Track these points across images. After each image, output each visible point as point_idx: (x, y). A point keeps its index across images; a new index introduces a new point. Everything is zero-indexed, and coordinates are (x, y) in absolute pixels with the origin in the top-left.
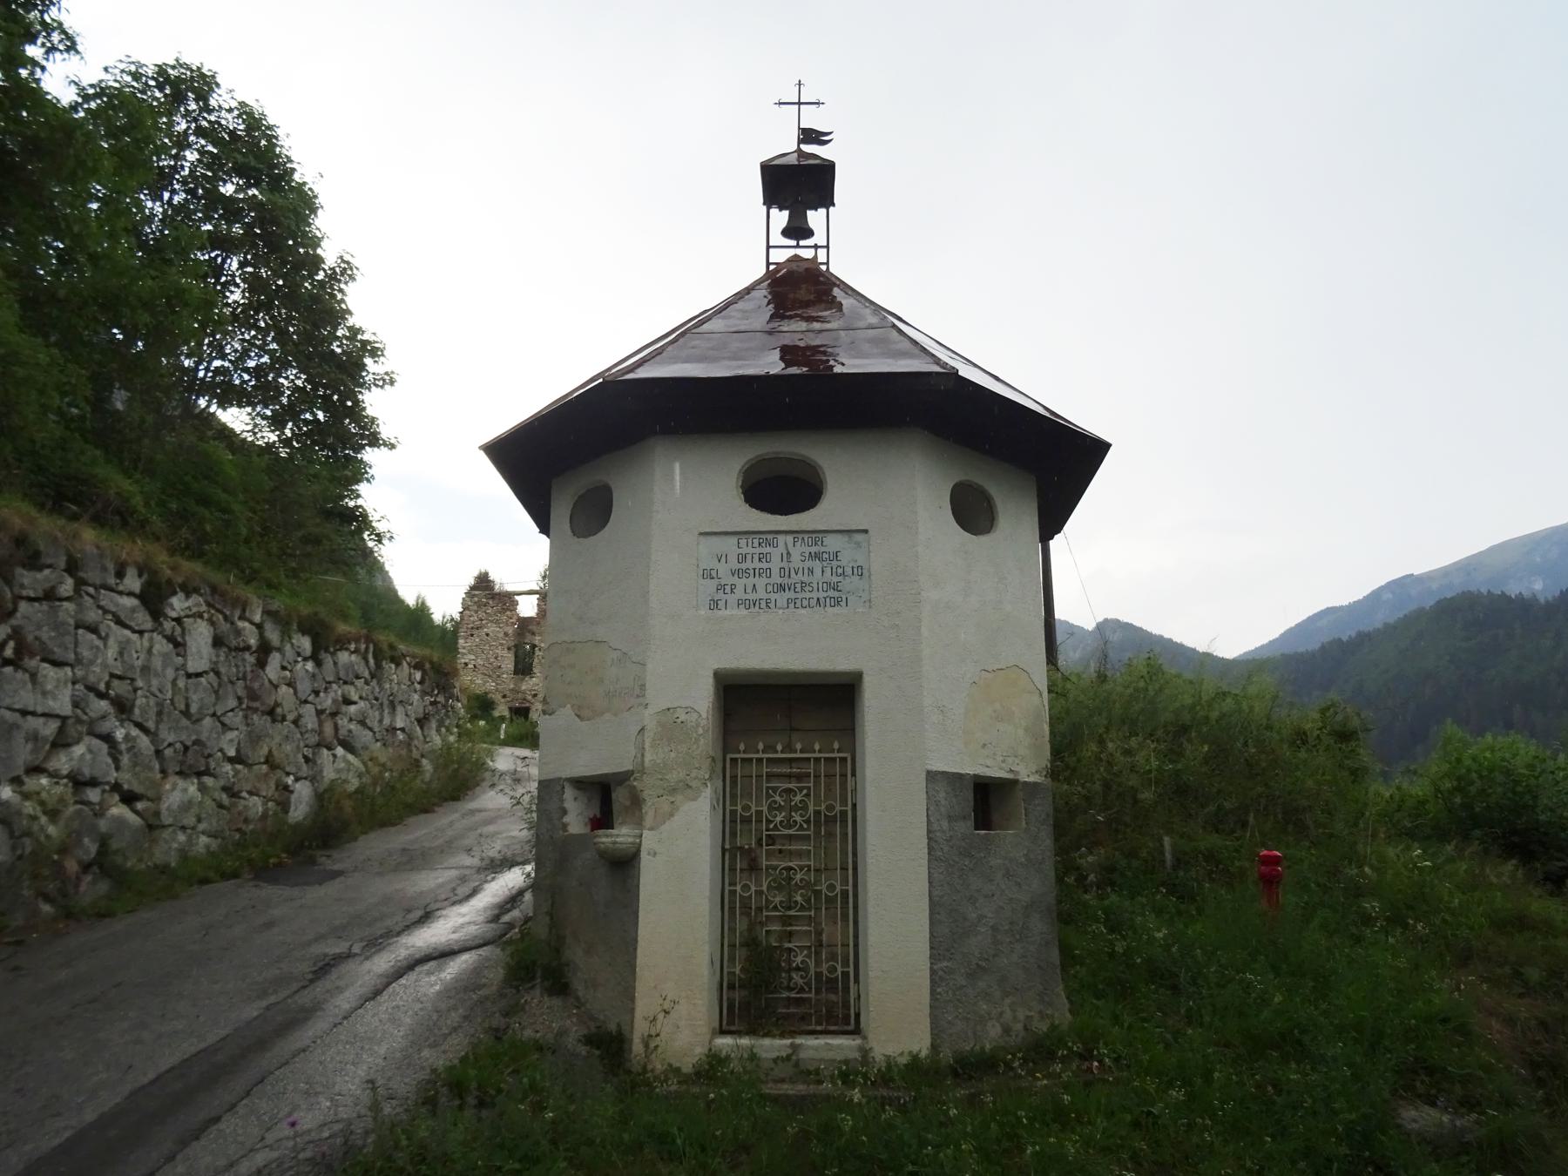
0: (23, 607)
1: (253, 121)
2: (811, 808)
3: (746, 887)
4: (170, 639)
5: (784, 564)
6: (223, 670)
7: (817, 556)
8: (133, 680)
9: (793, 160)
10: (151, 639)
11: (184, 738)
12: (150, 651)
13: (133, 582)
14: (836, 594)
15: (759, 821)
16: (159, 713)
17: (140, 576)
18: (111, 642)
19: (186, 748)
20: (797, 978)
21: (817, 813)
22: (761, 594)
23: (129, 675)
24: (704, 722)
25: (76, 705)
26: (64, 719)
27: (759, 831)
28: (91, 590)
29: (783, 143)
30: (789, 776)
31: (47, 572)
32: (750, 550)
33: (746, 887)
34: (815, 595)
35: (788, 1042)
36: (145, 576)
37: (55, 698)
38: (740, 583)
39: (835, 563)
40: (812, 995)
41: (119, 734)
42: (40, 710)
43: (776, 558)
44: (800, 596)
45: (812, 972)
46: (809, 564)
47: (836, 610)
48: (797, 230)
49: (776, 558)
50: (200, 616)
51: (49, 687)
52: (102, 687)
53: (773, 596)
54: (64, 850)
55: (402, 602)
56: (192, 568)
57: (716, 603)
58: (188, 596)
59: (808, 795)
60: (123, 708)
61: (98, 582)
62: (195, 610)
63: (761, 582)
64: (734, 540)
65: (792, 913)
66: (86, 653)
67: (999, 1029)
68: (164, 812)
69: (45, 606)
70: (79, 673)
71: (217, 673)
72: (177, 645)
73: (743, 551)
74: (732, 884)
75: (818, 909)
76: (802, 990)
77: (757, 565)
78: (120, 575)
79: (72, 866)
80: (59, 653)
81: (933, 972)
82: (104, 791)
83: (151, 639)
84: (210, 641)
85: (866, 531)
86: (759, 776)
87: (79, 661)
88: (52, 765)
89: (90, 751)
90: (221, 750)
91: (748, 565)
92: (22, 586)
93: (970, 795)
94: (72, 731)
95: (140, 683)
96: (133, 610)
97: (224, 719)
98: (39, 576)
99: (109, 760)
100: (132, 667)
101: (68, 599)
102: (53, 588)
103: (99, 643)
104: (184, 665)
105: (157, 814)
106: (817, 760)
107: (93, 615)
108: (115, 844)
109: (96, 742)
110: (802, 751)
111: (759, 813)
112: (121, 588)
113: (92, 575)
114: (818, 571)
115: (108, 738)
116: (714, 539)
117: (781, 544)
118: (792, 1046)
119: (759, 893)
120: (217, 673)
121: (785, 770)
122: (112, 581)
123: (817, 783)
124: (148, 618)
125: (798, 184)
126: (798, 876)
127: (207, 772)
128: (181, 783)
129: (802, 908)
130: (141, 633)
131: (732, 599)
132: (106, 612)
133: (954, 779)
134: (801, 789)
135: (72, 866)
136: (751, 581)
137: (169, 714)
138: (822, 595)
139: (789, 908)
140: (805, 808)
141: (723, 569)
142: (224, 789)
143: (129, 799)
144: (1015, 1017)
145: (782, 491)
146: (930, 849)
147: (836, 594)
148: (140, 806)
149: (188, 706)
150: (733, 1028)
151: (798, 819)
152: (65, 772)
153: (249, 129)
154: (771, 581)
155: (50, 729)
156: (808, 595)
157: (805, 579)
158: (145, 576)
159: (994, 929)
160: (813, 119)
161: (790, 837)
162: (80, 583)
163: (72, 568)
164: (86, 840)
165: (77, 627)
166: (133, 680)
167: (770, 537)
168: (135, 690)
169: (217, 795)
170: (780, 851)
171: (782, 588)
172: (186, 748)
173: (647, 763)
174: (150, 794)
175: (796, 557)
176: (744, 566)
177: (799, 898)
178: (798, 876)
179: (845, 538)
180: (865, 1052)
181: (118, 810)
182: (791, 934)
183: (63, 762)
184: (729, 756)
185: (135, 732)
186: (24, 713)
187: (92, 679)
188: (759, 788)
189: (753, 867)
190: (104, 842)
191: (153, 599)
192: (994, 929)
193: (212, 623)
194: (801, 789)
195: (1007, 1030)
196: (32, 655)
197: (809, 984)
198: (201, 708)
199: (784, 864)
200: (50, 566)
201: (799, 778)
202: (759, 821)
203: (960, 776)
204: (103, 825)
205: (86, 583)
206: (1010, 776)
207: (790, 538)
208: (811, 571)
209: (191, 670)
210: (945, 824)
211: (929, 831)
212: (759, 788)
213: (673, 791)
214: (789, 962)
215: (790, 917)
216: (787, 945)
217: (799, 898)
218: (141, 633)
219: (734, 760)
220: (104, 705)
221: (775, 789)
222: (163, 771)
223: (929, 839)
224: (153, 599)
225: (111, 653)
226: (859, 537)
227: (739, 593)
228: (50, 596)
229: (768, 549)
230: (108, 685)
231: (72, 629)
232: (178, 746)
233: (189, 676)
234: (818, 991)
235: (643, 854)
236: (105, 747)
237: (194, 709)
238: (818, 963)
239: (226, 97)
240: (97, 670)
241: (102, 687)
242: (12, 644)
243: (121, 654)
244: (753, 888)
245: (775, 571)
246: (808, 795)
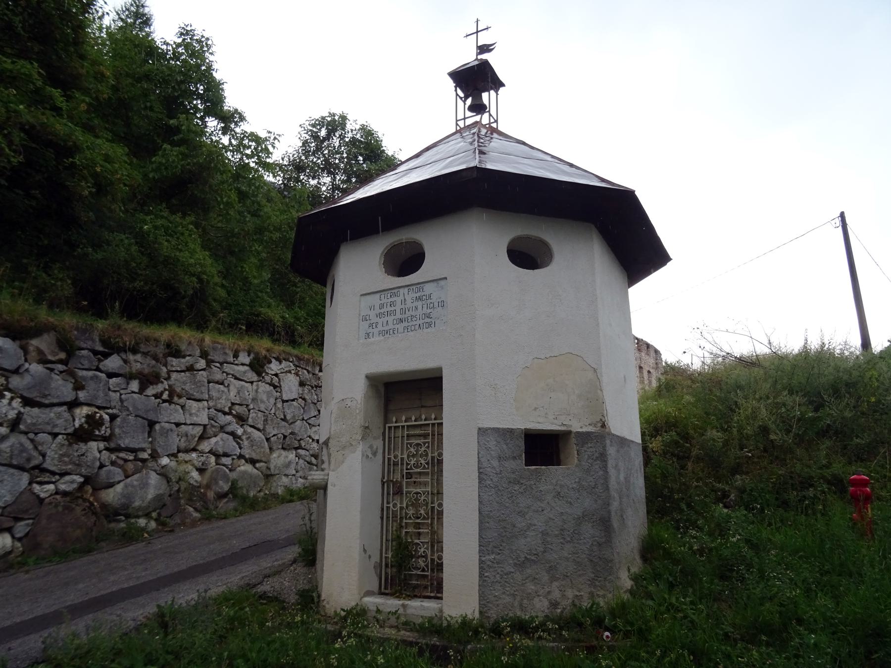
0: (174, 376)
1: (367, 132)
2: (430, 455)
3: (395, 505)
4: (271, 384)
5: (403, 306)
6: (307, 397)
7: (419, 299)
8: (247, 406)
9: (477, 63)
10: (257, 385)
11: (283, 431)
12: (257, 391)
13: (244, 358)
14: (429, 320)
15: (402, 464)
16: (266, 420)
17: (249, 355)
18: (231, 387)
19: (285, 437)
20: (421, 563)
21: (433, 458)
22: (391, 326)
23: (244, 403)
24: (359, 406)
25: (210, 418)
26: (205, 426)
27: (402, 470)
28: (218, 365)
29: (467, 56)
30: (420, 435)
31: (188, 358)
32: (386, 301)
33: (395, 505)
34: (418, 322)
35: (401, 602)
36: (252, 356)
37: (197, 416)
38: (380, 321)
39: (429, 301)
40: (429, 574)
41: (240, 431)
42: (188, 422)
43: (399, 303)
44: (410, 324)
45: (429, 559)
46: (416, 304)
47: (429, 330)
48: (478, 108)
49: (399, 303)
50: (290, 372)
51: (194, 411)
52: (227, 410)
53: (396, 326)
54: (208, 487)
55: (842, 358)
56: (279, 348)
57: (368, 334)
58: (280, 362)
59: (428, 447)
60: (241, 420)
61: (221, 361)
62: (287, 369)
63: (390, 319)
64: (378, 295)
65: (418, 521)
66: (214, 394)
67: (546, 603)
68: (272, 467)
69: (188, 374)
70: (211, 404)
71: (304, 399)
72: (275, 387)
73: (382, 302)
74: (388, 503)
75: (433, 519)
76: (423, 570)
77: (389, 309)
78: (236, 356)
79: (211, 495)
80: (197, 395)
81: (481, 562)
82: (233, 459)
83: (257, 385)
84: (297, 383)
85: (446, 278)
86: (403, 437)
87: (211, 398)
88: (200, 448)
89: (222, 439)
90: (310, 437)
91: (385, 310)
92: (172, 366)
93: (522, 444)
94: (210, 431)
95: (251, 406)
96: (245, 372)
97: (309, 421)
98: (183, 360)
99: (235, 444)
100: (245, 399)
101: (204, 370)
102: (192, 366)
103: (226, 390)
104: (281, 396)
105: (268, 468)
106: (433, 424)
107: (218, 376)
108: (240, 484)
109: (225, 435)
110: (415, 421)
111: (402, 459)
112: (236, 362)
113: (216, 356)
114: (420, 307)
115: (233, 434)
116: (368, 297)
117: (402, 295)
118: (404, 606)
119: (402, 508)
120: (304, 399)
121: (418, 432)
122: (231, 359)
123: (433, 439)
124: (255, 375)
125: (476, 80)
126: (422, 498)
127: (300, 447)
128: (284, 453)
129: (424, 518)
130: (252, 383)
131: (376, 331)
132: (228, 374)
133: (507, 434)
134: (425, 443)
135: (211, 495)
136: (386, 318)
137: (272, 420)
138: (421, 322)
139: (418, 518)
140: (427, 455)
141: (372, 314)
142: (312, 455)
143: (253, 462)
144: (563, 596)
145: (406, 262)
146: (481, 480)
147: (429, 320)
148: (257, 465)
149: (285, 416)
150: (387, 591)
151: (423, 462)
152: (207, 451)
153: (367, 137)
154: (396, 317)
155: (198, 430)
156: (414, 323)
157: (413, 313)
158: (252, 356)
159: (544, 534)
160: (484, 39)
161: (420, 473)
162: (209, 363)
163: (204, 355)
164: (221, 482)
165: (209, 382)
166: (247, 406)
167: (396, 291)
168: (249, 411)
169: (307, 459)
170: (415, 482)
171: (401, 321)
172: (285, 437)
173: (332, 433)
174: (263, 459)
175: (409, 301)
176: (382, 311)
177: (422, 512)
178: (422, 498)
179: (435, 284)
180: (441, 611)
181: (248, 468)
182: (419, 534)
183: (205, 446)
184: (387, 425)
185: (250, 430)
186: (178, 425)
187: (219, 406)
188: (402, 443)
189: (399, 492)
190: (234, 484)
191: (258, 366)
192: (544, 534)
193: (297, 374)
194: (425, 443)
195: (554, 604)
196: (180, 397)
197: (427, 566)
198: (294, 416)
199: (415, 491)
200: (189, 355)
201: (425, 436)
202: (402, 464)
203: (511, 431)
204: (233, 475)
205: (213, 361)
206: (563, 428)
207: (406, 289)
208: (416, 308)
209: (285, 398)
210: (495, 463)
211: (479, 468)
212: (402, 443)
213: (344, 448)
214: (416, 551)
215: (419, 523)
216: (417, 541)
217: (422, 512)
218: (252, 383)
219: (390, 428)
220: (229, 418)
221: (411, 444)
222: (271, 449)
223: (480, 473)
224: (258, 366)
225: (233, 393)
226: (442, 283)
227: (380, 328)
228: (191, 369)
229: (395, 299)
230: (230, 408)
231: (206, 384)
232: (280, 436)
233: (284, 401)
234: (432, 570)
235: (329, 486)
236: (231, 438)
237: (288, 417)
238: (432, 555)
239: (354, 124)
240: (223, 402)
241: (227, 410)
242: (167, 392)
243: (238, 393)
244: (399, 505)
245: (398, 311)
246: (428, 447)
